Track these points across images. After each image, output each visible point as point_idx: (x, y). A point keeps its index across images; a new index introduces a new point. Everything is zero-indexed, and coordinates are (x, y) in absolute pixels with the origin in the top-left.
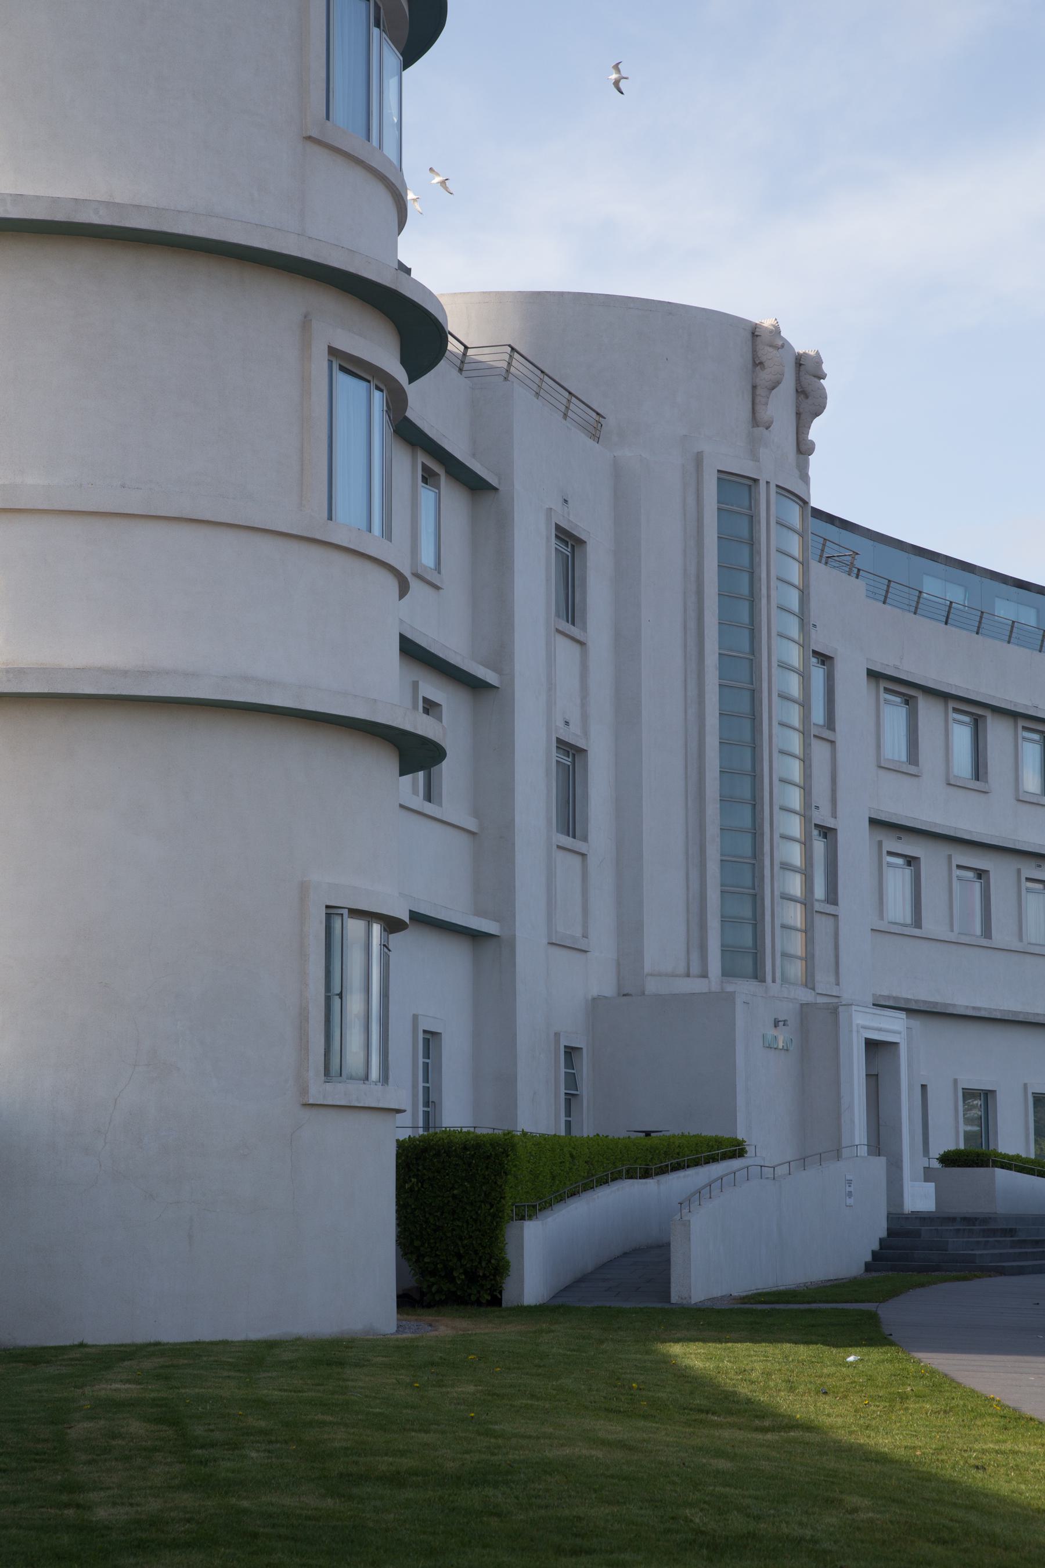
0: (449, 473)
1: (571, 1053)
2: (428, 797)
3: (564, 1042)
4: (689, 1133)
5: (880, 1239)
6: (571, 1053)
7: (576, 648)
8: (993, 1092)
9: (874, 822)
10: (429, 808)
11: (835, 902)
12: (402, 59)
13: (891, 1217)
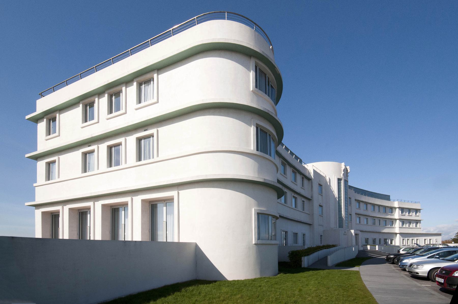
0: (305, 178)
1: (321, 236)
2: (303, 210)
3: (320, 234)
4: (312, 246)
5: (389, 196)
6: (321, 236)
7: (321, 196)
8: (297, 233)
9: (356, 214)
10: (303, 211)
11: (351, 221)
12: (331, 188)
13: (358, 250)
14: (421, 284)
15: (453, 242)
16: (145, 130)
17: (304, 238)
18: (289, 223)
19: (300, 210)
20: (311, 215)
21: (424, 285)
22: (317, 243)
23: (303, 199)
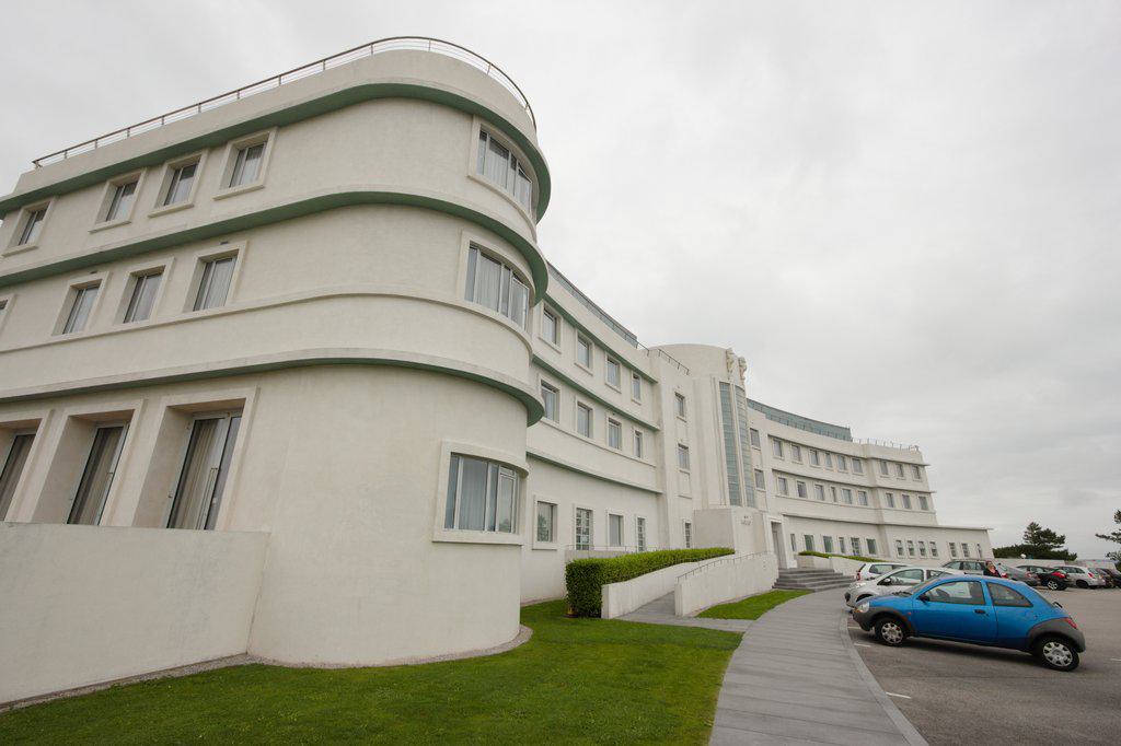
1: (688, 525)
6: (688, 525)
14: (883, 689)
15: (1023, 555)
16: (223, 243)
17: (640, 529)
18: (627, 495)
19: (812, 499)
20: (660, 469)
21: (892, 691)
22: (677, 543)
23: (831, 485)
